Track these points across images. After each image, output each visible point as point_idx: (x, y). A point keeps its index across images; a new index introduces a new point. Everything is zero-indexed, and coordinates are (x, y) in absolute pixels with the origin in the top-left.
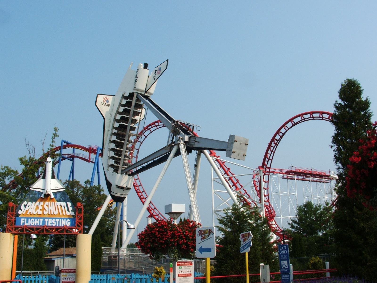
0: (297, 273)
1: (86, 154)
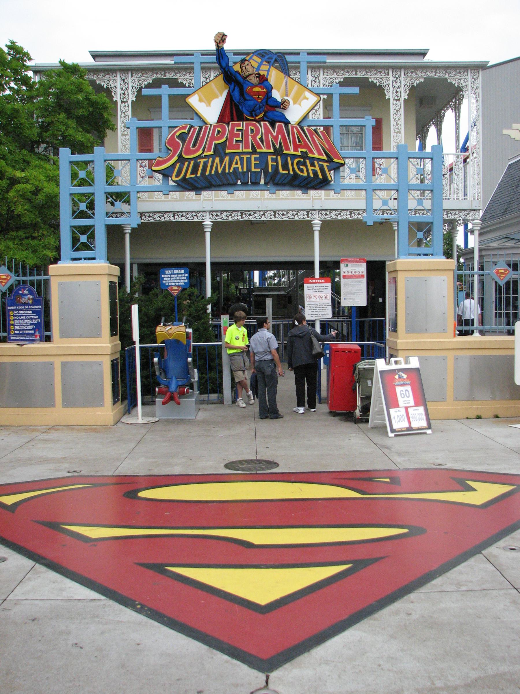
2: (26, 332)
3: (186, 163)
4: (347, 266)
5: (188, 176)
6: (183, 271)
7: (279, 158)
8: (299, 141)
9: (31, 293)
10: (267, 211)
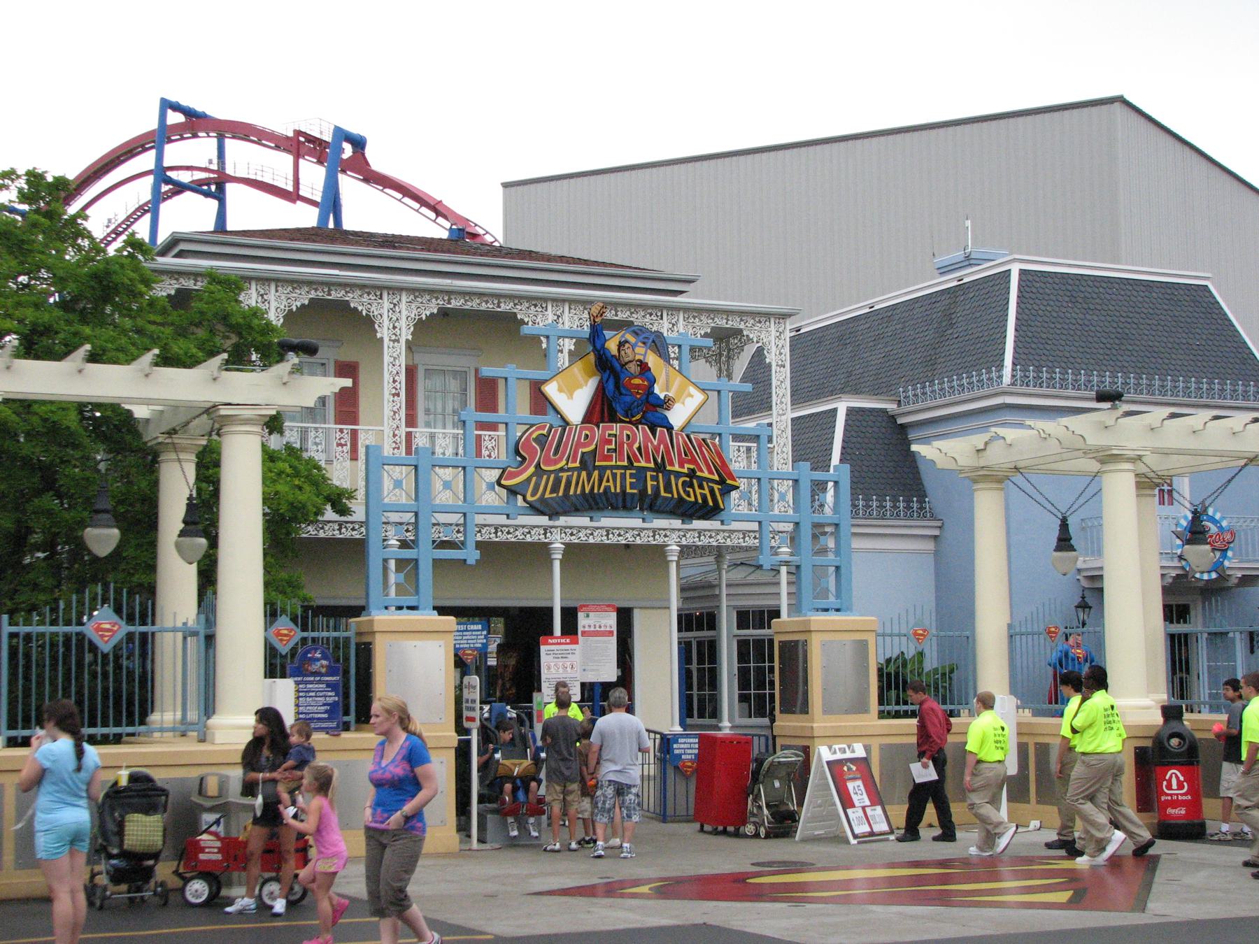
0: (878, 546)
1: (277, 167)
2: (316, 716)
3: (545, 477)
4: (588, 616)
5: (547, 495)
6: (480, 627)
7: (660, 475)
8: (686, 455)
9: (324, 657)
10: (485, 526)
